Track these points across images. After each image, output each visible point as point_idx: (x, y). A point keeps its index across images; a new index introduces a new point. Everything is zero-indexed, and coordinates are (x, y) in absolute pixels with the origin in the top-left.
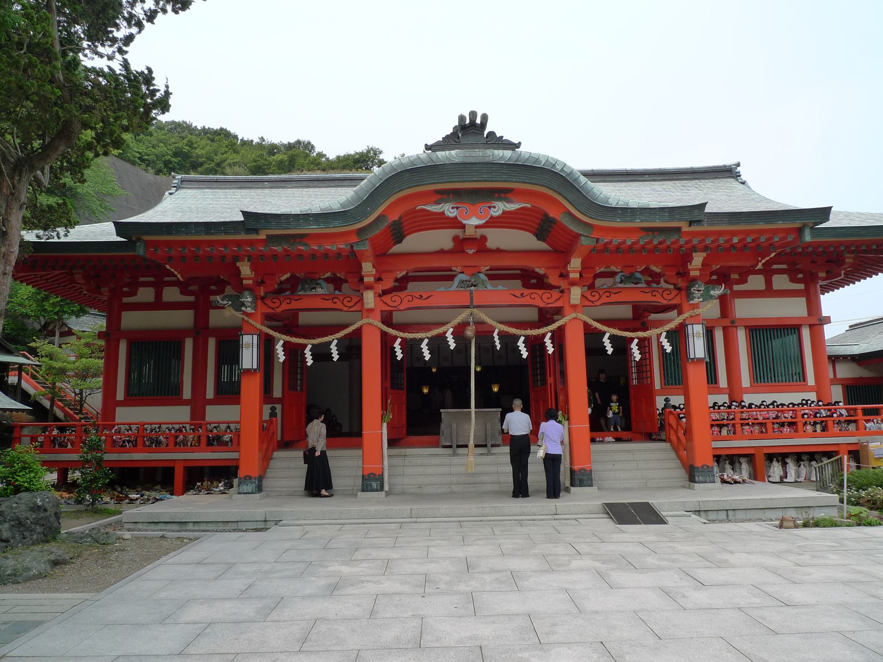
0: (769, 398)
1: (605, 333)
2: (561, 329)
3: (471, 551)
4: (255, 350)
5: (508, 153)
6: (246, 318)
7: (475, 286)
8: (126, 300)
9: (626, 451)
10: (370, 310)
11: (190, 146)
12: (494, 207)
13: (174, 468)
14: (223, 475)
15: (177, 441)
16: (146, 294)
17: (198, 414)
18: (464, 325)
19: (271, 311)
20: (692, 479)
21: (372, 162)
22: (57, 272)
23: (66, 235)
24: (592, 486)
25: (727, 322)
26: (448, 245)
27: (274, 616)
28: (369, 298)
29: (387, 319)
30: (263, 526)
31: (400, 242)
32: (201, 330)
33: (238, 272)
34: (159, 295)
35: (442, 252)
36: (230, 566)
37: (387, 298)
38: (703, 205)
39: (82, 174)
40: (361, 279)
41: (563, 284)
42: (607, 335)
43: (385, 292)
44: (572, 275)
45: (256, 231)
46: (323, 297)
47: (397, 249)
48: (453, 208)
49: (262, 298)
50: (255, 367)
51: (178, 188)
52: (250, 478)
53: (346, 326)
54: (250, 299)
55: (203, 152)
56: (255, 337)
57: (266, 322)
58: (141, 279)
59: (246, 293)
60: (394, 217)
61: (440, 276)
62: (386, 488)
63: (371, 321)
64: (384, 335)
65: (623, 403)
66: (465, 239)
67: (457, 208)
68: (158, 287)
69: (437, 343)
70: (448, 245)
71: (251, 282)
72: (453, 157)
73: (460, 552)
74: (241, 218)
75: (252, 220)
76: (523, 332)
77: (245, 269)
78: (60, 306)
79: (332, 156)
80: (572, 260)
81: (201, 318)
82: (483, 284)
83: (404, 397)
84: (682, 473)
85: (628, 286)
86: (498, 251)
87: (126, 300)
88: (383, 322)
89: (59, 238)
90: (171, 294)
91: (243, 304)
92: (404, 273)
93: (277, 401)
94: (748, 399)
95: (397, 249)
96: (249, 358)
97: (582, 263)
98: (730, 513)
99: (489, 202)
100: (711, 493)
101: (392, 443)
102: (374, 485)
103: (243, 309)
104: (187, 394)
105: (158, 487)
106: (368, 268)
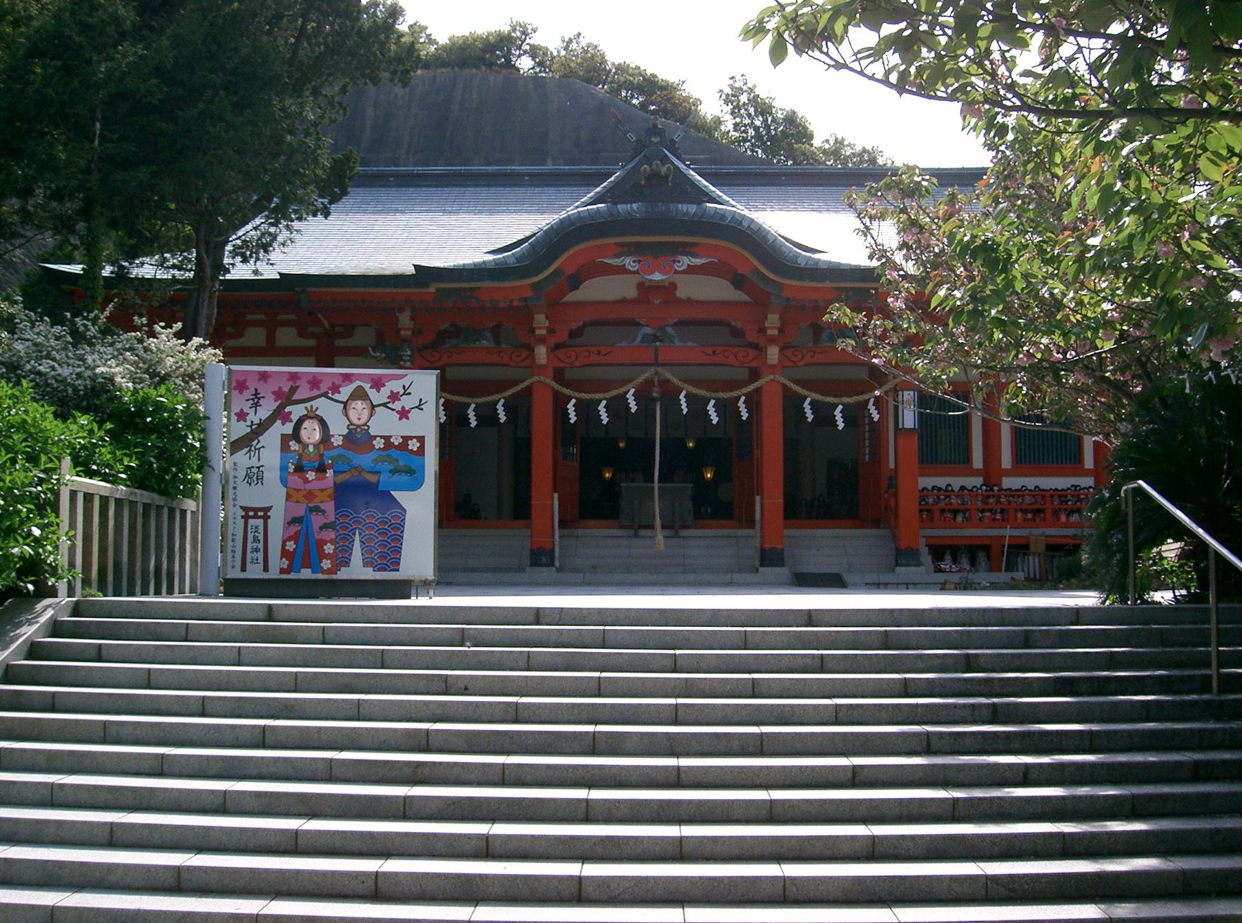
0: (1031, 482)
1: (806, 398)
2: (758, 391)
8: (340, 343)
18: (648, 384)
21: (519, 48)
24: (783, 566)
26: (632, 293)
28: (541, 353)
29: (559, 376)
31: (577, 288)
34: (271, 337)
35: (624, 301)
37: (561, 353)
40: (532, 331)
42: (808, 400)
43: (557, 347)
47: (572, 297)
53: (515, 383)
58: (249, 317)
62: (557, 564)
64: (556, 394)
67: (639, 262)
68: (271, 327)
70: (632, 293)
71: (409, 333)
74: (412, 271)
77: (405, 319)
86: (689, 300)
94: (1009, 483)
95: (572, 297)
101: (563, 524)
102: (544, 560)
106: (541, 321)
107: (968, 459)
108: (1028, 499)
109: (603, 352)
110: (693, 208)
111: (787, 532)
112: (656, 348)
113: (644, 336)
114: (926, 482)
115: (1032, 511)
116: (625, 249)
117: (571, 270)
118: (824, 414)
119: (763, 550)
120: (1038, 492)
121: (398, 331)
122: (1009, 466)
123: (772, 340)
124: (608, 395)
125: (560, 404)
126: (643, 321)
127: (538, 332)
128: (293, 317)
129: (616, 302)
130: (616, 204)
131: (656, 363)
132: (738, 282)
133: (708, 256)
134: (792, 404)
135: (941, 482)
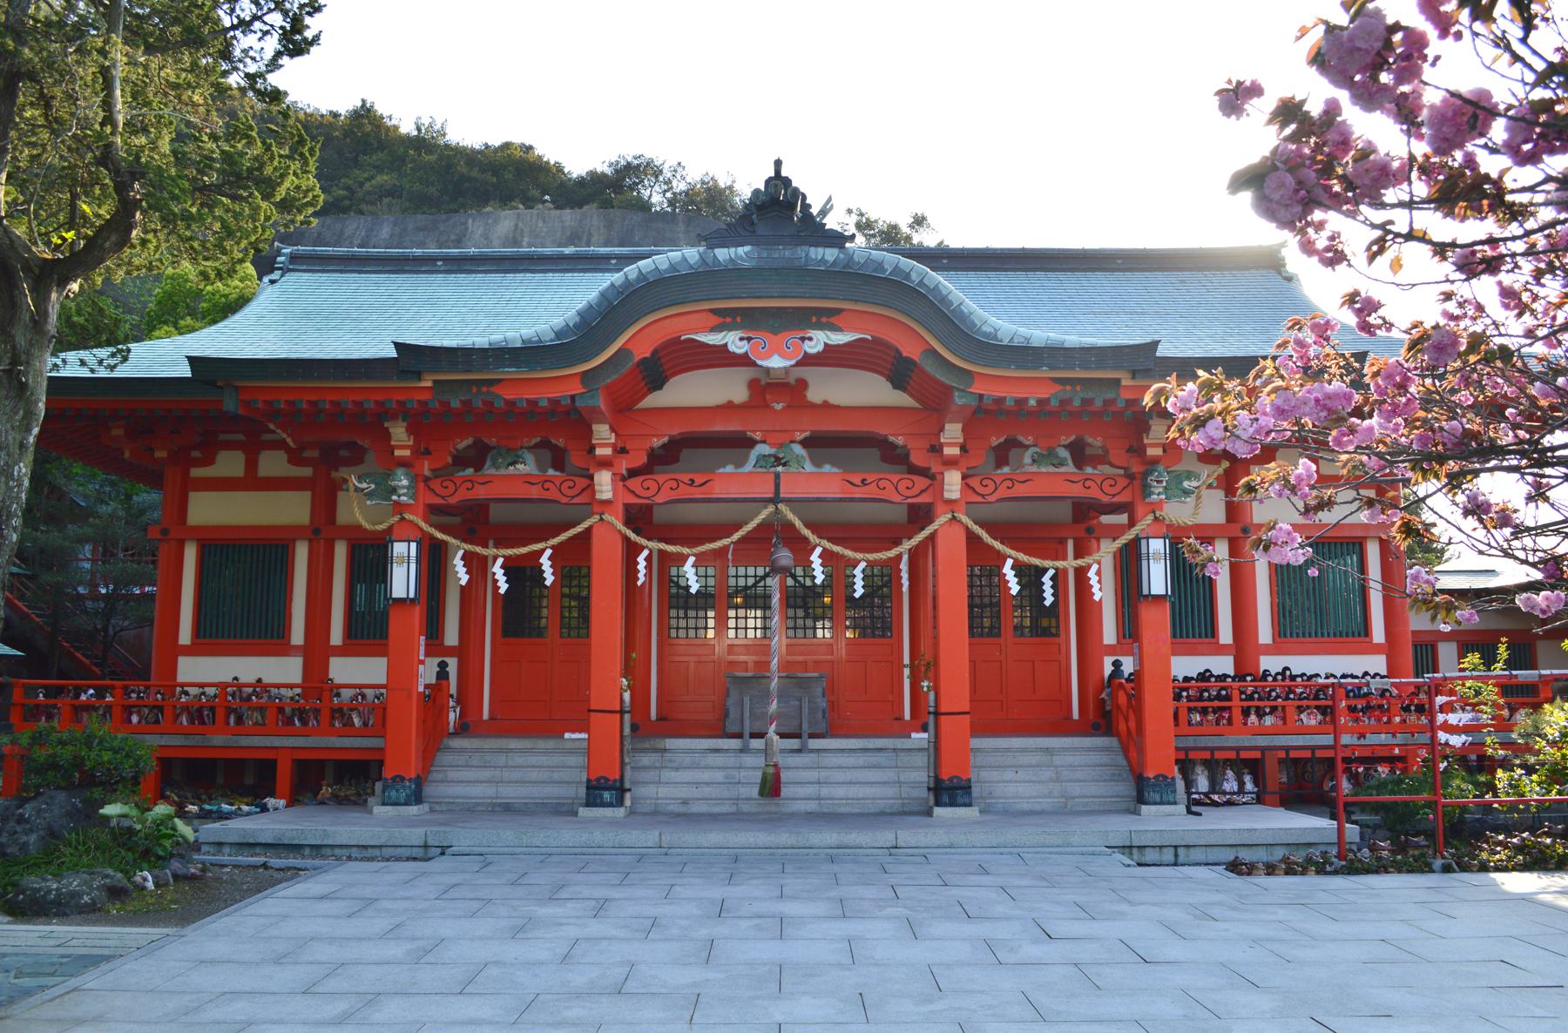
3: (734, 892)
4: (413, 567)
5: (831, 254)
7: (784, 465)
12: (810, 339)
16: (230, 464)
20: (1141, 800)
24: (970, 805)
25: (1236, 531)
26: (740, 394)
27: (430, 958)
30: (424, 853)
31: (660, 387)
32: (323, 528)
33: (387, 435)
34: (252, 464)
35: (729, 406)
36: (372, 901)
37: (634, 483)
38: (1156, 344)
40: (592, 448)
43: (633, 473)
44: (947, 451)
46: (527, 480)
49: (427, 479)
50: (412, 595)
51: (285, 271)
52: (402, 779)
54: (405, 482)
56: (413, 545)
58: (222, 437)
59: (400, 472)
64: (626, 539)
66: (769, 385)
67: (749, 339)
70: (740, 394)
71: (407, 453)
72: (741, 258)
73: (717, 893)
74: (392, 353)
75: (412, 357)
79: (576, 167)
80: (947, 427)
81: (326, 505)
84: (1127, 788)
86: (826, 405)
87: (196, 472)
88: (627, 523)
91: (394, 490)
93: (450, 651)
94: (1271, 664)
96: (403, 581)
98: (1181, 851)
100: (1164, 820)
104: (298, 636)
106: (603, 433)
107: (1213, 631)
109: (699, 480)
111: (976, 743)
112: (777, 476)
116: (727, 319)
117: (643, 351)
122: (1269, 641)
123: (951, 463)
124: (510, 552)
125: (632, 550)
126: (758, 436)
127: (599, 451)
128: (241, 437)
129: (718, 407)
130: (711, 247)
131: (775, 500)
132: (900, 372)
133: (855, 330)
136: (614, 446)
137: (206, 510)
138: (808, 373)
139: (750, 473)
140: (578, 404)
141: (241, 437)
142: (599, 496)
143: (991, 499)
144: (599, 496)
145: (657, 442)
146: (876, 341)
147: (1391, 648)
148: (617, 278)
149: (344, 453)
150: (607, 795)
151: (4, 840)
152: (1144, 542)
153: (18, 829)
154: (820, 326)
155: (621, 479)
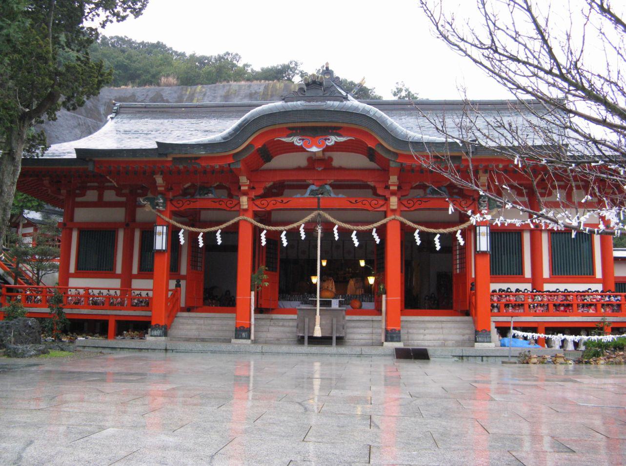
0: (562, 287)
1: (415, 229)
2: (384, 226)
4: (164, 236)
6: (159, 214)
7: (322, 194)
8: (78, 199)
9: (438, 321)
10: (245, 210)
11: (129, 60)
12: (329, 139)
13: (108, 321)
14: (141, 327)
15: (109, 302)
16: (92, 196)
17: (126, 286)
19: (177, 209)
22: (31, 178)
23: (42, 156)
24: (400, 341)
26: (304, 163)
28: (244, 200)
34: (101, 196)
35: (299, 169)
37: (258, 202)
39: (55, 115)
41: (387, 193)
42: (417, 231)
44: (392, 188)
45: (166, 155)
47: (267, 166)
48: (300, 140)
49: (171, 200)
50: (164, 248)
54: (161, 201)
55: (141, 65)
56: (165, 228)
57: (173, 217)
58: (89, 184)
59: (159, 196)
60: (259, 145)
61: (293, 185)
62: (252, 337)
63: (245, 218)
65: (437, 285)
67: (303, 140)
68: (101, 190)
69: (293, 235)
71: (162, 189)
74: (156, 146)
76: (355, 227)
77: (159, 180)
78: (23, 202)
79: (257, 66)
80: (391, 177)
82: (328, 193)
83: (277, 279)
85: (435, 196)
86: (341, 169)
87: (78, 199)
89: (38, 157)
90: (110, 196)
91: (157, 204)
92: (271, 183)
93: (184, 277)
94: (547, 287)
97: (398, 179)
99: (325, 136)
101: (259, 310)
103: (157, 207)
104: (119, 270)
105: (97, 335)
106: (243, 180)
107: (521, 271)
108: (561, 297)
109: (284, 202)
110: (337, 103)
111: (403, 318)
112: (319, 199)
113: (312, 191)
114: (495, 286)
115: (563, 305)
118: (427, 238)
119: (387, 331)
120: (567, 293)
121: (156, 187)
125: (257, 232)
127: (243, 188)
128: (96, 184)
131: (318, 208)
133: (348, 136)
134: (406, 233)
135: (504, 286)
136: (248, 186)
137: (82, 215)
138: (328, 154)
139: (307, 198)
140: (232, 167)
141: (96, 184)
142: (242, 207)
143: (412, 209)
144: (242, 207)
145: (268, 185)
146: (356, 140)
147: (603, 281)
148: (308, 104)
149: (139, 191)
150: (244, 335)
151: (2, 334)
152: (478, 228)
153: (7, 331)
154: (333, 135)
155: (251, 200)
